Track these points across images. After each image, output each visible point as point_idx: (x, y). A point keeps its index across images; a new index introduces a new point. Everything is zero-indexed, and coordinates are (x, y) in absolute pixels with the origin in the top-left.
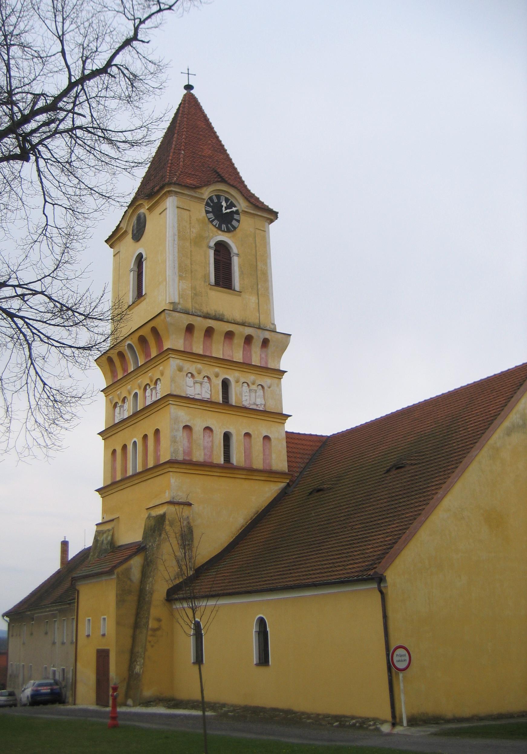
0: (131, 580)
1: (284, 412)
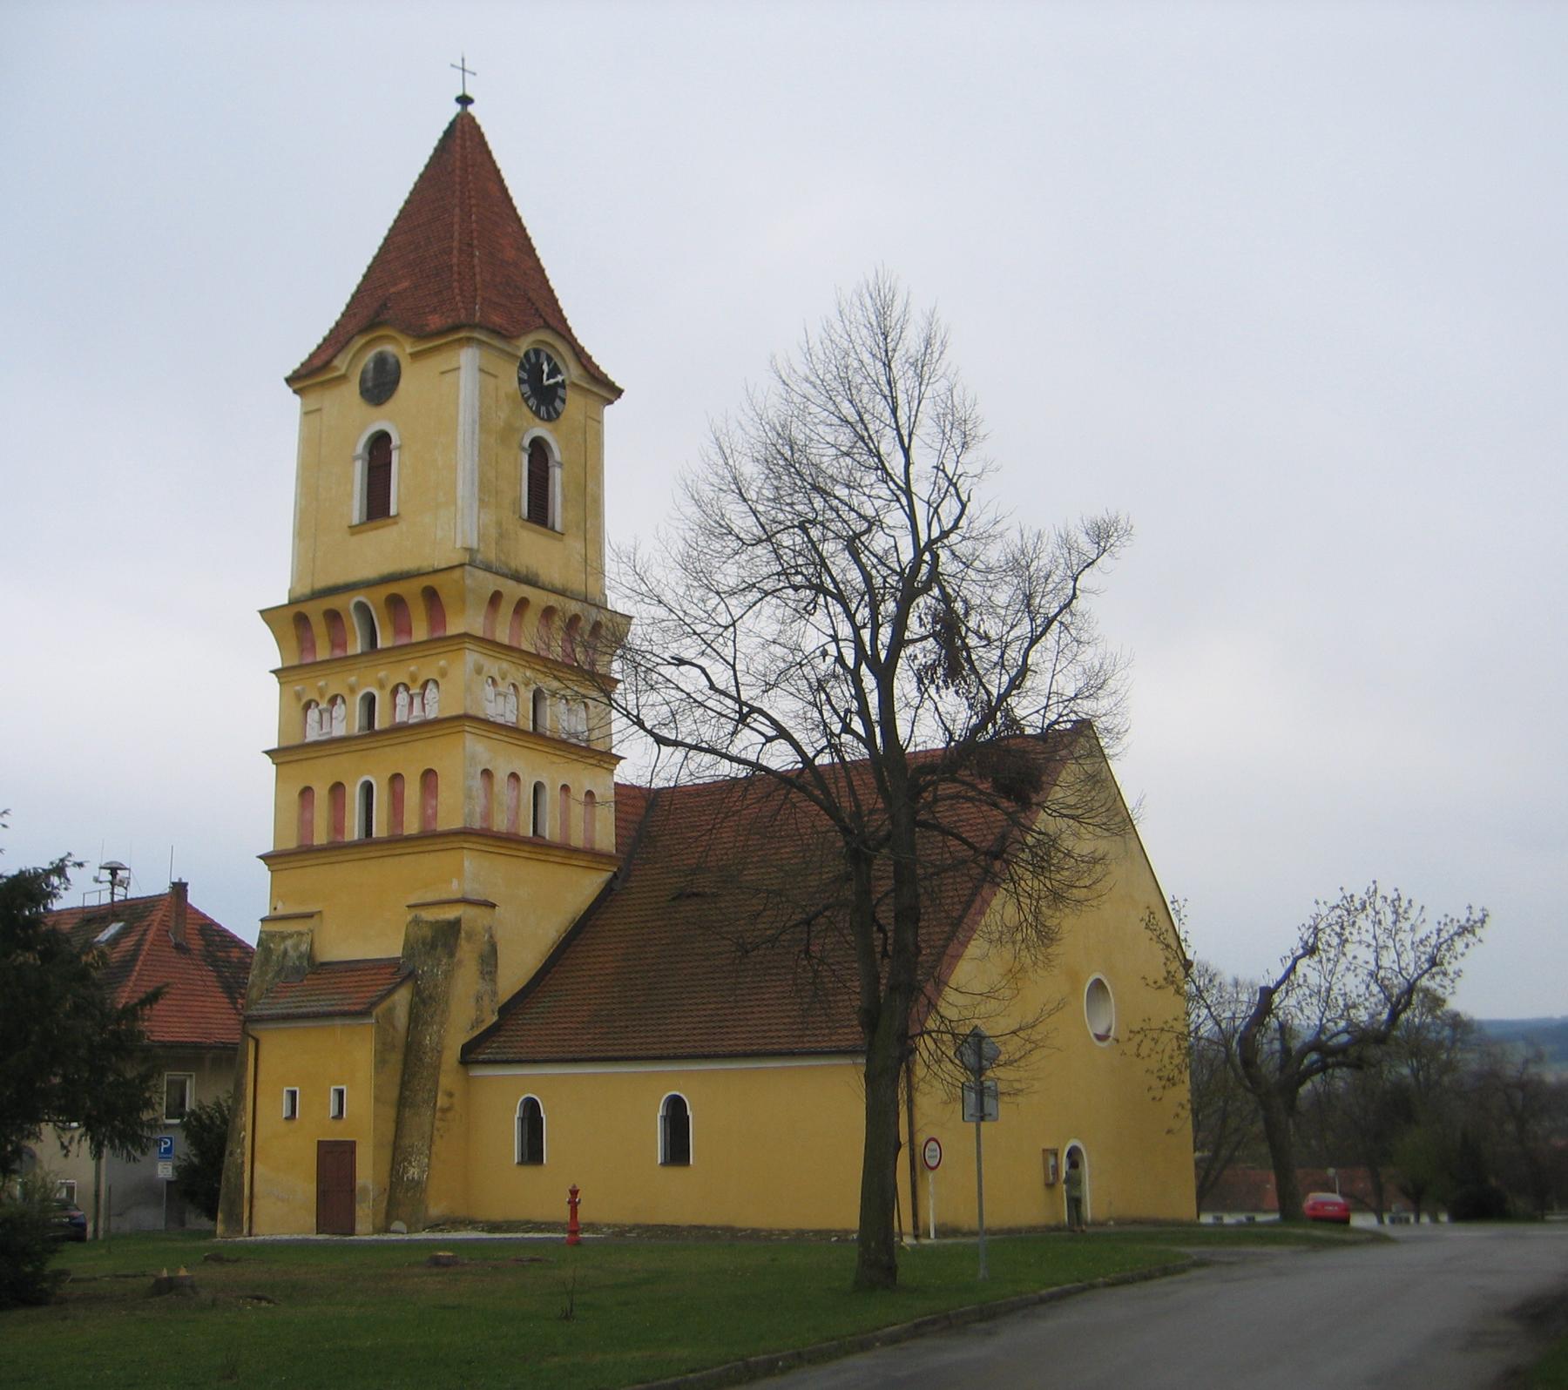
0: (394, 1027)
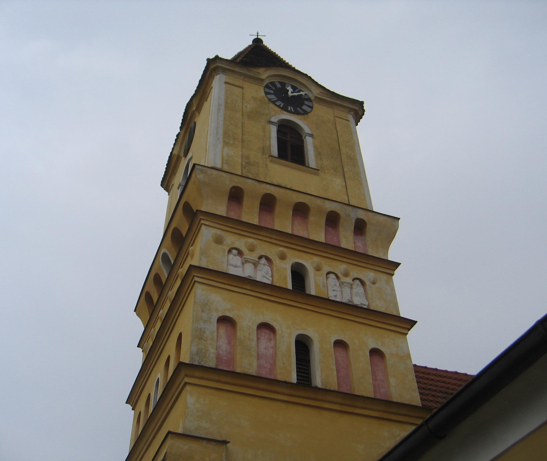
1: (404, 313)
